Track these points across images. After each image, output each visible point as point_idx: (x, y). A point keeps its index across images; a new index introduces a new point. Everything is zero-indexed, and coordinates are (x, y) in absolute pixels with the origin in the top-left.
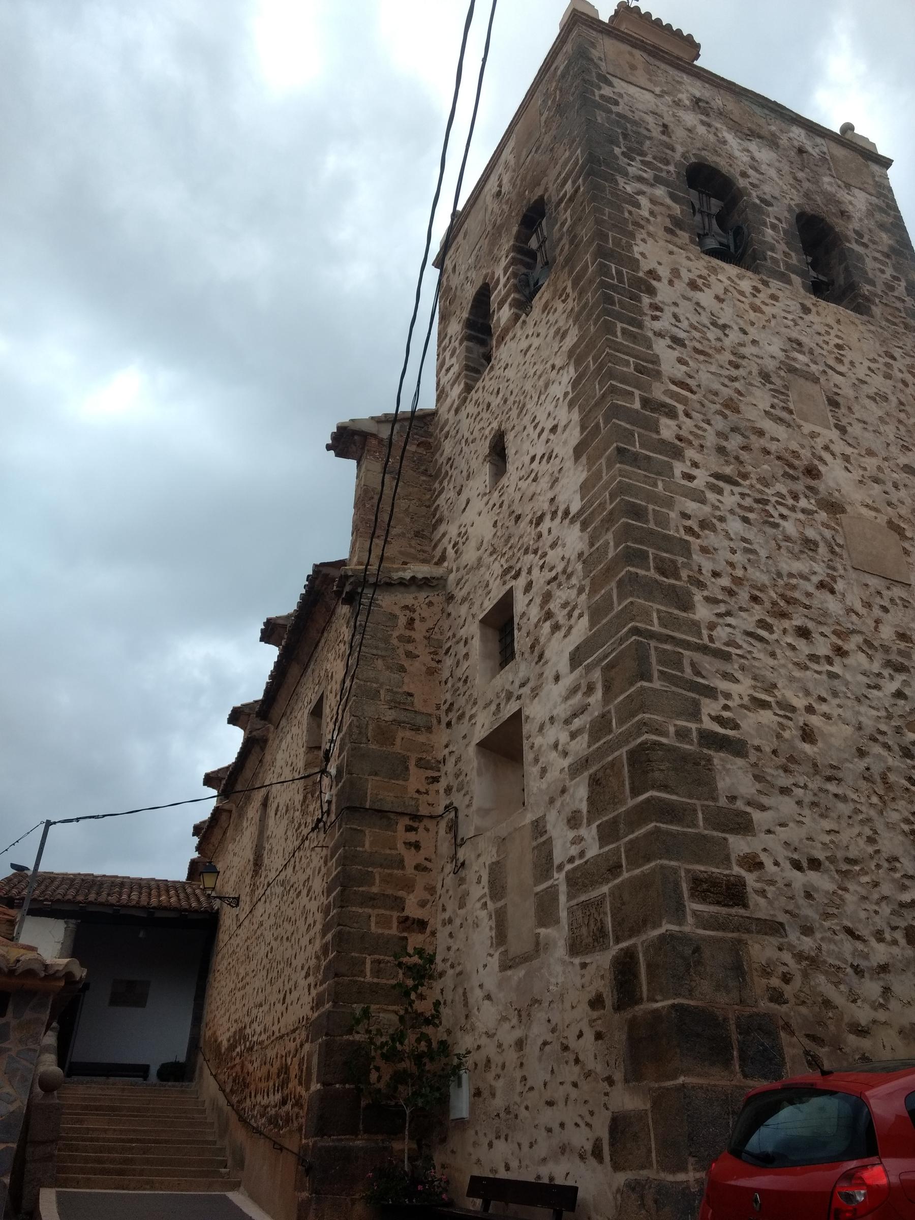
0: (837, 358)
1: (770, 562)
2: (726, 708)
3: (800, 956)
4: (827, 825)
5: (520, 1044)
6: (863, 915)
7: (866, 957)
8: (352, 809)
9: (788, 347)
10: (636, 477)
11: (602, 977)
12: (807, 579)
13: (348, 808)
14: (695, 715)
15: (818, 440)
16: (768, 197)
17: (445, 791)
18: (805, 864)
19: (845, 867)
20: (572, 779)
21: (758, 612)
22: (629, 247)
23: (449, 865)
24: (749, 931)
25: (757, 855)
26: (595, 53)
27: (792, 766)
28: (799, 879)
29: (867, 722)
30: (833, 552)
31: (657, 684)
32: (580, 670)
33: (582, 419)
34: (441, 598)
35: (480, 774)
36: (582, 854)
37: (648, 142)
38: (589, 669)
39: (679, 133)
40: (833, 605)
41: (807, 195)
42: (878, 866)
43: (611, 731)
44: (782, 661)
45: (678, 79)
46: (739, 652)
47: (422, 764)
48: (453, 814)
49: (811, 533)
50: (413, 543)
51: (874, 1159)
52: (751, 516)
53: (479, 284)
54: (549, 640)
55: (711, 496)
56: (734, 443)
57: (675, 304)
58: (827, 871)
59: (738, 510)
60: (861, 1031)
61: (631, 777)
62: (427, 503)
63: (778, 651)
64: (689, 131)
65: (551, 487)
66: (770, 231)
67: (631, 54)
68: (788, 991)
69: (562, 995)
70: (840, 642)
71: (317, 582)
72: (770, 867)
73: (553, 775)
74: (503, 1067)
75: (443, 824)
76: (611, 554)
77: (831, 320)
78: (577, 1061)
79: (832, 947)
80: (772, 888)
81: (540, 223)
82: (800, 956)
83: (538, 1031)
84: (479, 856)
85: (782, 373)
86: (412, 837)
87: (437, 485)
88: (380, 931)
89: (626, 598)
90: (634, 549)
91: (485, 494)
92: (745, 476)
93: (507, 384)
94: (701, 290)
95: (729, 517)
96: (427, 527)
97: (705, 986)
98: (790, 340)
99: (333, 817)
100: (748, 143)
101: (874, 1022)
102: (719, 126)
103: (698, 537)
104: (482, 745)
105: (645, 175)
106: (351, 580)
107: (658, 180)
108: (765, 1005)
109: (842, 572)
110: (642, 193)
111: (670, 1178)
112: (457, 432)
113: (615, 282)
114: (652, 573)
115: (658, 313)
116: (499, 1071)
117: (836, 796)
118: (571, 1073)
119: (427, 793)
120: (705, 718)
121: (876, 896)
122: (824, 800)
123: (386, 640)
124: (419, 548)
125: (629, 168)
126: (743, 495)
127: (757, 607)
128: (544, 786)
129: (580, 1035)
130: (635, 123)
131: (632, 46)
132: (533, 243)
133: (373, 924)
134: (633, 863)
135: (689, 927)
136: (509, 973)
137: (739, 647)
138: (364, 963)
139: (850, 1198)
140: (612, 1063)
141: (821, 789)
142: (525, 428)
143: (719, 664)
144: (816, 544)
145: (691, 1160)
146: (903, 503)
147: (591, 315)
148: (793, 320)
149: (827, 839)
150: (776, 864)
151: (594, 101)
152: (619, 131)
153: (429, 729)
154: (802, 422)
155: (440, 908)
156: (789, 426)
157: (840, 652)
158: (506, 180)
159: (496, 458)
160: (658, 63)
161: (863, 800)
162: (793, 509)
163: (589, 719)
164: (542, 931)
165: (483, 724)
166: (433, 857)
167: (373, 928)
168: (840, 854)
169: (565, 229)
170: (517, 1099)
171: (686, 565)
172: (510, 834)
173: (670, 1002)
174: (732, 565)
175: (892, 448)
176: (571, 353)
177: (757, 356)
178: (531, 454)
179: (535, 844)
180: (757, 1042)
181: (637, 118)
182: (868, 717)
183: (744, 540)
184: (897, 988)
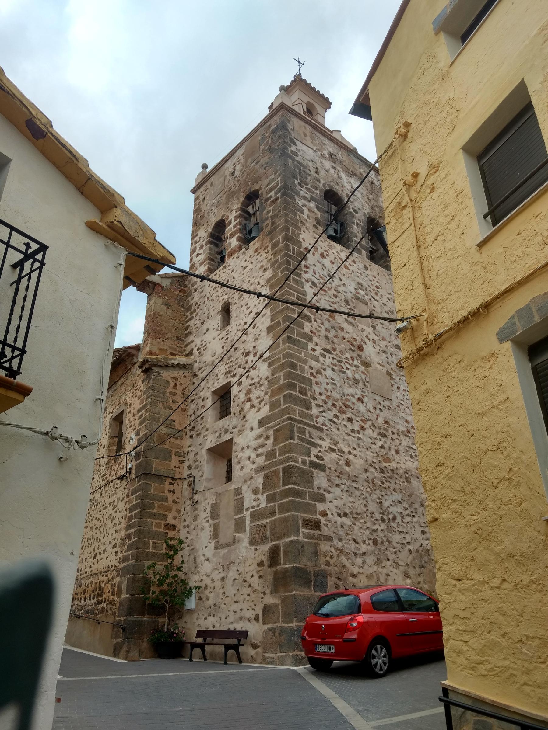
0: (376, 293)
1: (341, 389)
2: (320, 451)
3: (337, 549)
4: (351, 499)
5: (223, 579)
6: (360, 534)
7: (359, 549)
8: (146, 474)
9: (357, 287)
10: (294, 349)
11: (264, 554)
12: (354, 397)
13: (144, 473)
14: (308, 454)
15: (364, 333)
16: (356, 209)
17: (188, 467)
18: (342, 515)
19: (355, 516)
20: (256, 474)
21: (335, 411)
22: (298, 237)
23: (189, 501)
24: (320, 540)
25: (326, 511)
26: (290, 126)
27: (341, 476)
28: (339, 520)
29: (370, 458)
30: (364, 385)
31: (296, 441)
32: (262, 429)
33: (272, 315)
34: (190, 374)
35: (207, 463)
36: (258, 505)
37: (309, 177)
38: (267, 429)
39: (323, 173)
40: (362, 408)
41: (372, 208)
42: (367, 516)
43: (275, 458)
44: (341, 432)
45: (324, 142)
46: (326, 428)
47: (178, 454)
48: (192, 479)
49: (357, 376)
50: (176, 342)
51: (360, 614)
52: (336, 368)
53: (219, 218)
54: (249, 411)
55: (321, 359)
56: (331, 335)
57: (315, 265)
58: (349, 517)
59: (331, 365)
60: (354, 576)
61: (283, 478)
62: (183, 322)
63: (340, 428)
64: (327, 171)
65: (254, 341)
66: (355, 227)
67: (305, 127)
68: (332, 562)
69: (245, 561)
70: (363, 424)
71: (124, 355)
72: (330, 516)
73: (246, 471)
74: (214, 588)
75: (186, 483)
76: (282, 382)
77: (375, 274)
78: (250, 586)
79: (348, 546)
80: (330, 524)
81: (255, 201)
82: (337, 549)
83: (232, 574)
84: (206, 499)
85: (354, 300)
86: (172, 488)
87: (188, 314)
88: (156, 529)
89: (287, 404)
90: (291, 383)
91: (218, 330)
92: (334, 350)
93: (233, 280)
94: (325, 258)
95: (327, 368)
96: (183, 334)
97: (304, 560)
98: (358, 284)
99: (133, 476)
100: (351, 178)
101: (359, 573)
102: (339, 169)
103: (315, 377)
104: (210, 450)
105: (307, 196)
106: (150, 363)
107: (313, 199)
108: (324, 567)
109: (367, 394)
110: (304, 205)
111: (286, 625)
112: (202, 291)
113: (291, 254)
114: (297, 393)
115: (307, 270)
116: (212, 590)
117: (355, 488)
118: (248, 590)
119: (179, 468)
120: (312, 456)
121: (365, 527)
122: (351, 489)
123: (164, 393)
124: (178, 345)
125: (301, 192)
126: (333, 358)
127: (334, 409)
128: (242, 475)
129: (252, 576)
130: (304, 167)
131: (306, 123)
132: (250, 209)
133: (153, 527)
134: (281, 512)
135: (301, 538)
136: (219, 550)
137: (326, 426)
138: (149, 543)
139: (352, 625)
140: (266, 587)
141: (350, 485)
142: (242, 306)
143: (319, 433)
144: (358, 381)
145: (295, 619)
146: (393, 363)
147: (280, 267)
148: (360, 273)
149: (350, 505)
150: (332, 514)
151: (288, 154)
152: (298, 171)
153: (181, 438)
154: (359, 324)
155: (183, 520)
156: (354, 326)
157: (363, 428)
158: (238, 168)
159: (224, 313)
160: (316, 132)
161: (364, 490)
162: (351, 365)
163: (266, 450)
164: (237, 535)
165: (211, 441)
166: (180, 497)
167: (154, 528)
168: (354, 511)
169: (269, 215)
170: (220, 601)
171: (310, 390)
172: (223, 492)
173: (292, 565)
174: (326, 390)
175: (393, 337)
176: (268, 281)
177: (345, 292)
178: (245, 320)
179: (235, 498)
180: (319, 579)
181: (305, 164)
182: (370, 456)
183: (332, 379)
184: (368, 561)
